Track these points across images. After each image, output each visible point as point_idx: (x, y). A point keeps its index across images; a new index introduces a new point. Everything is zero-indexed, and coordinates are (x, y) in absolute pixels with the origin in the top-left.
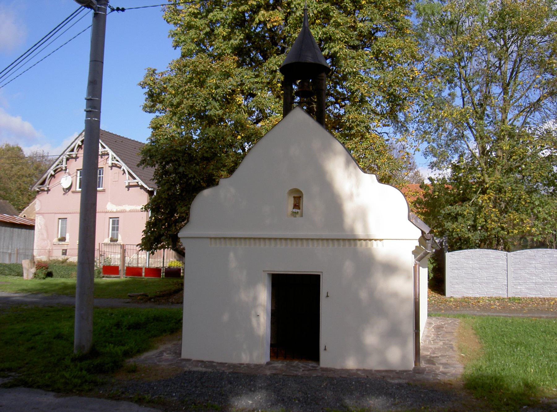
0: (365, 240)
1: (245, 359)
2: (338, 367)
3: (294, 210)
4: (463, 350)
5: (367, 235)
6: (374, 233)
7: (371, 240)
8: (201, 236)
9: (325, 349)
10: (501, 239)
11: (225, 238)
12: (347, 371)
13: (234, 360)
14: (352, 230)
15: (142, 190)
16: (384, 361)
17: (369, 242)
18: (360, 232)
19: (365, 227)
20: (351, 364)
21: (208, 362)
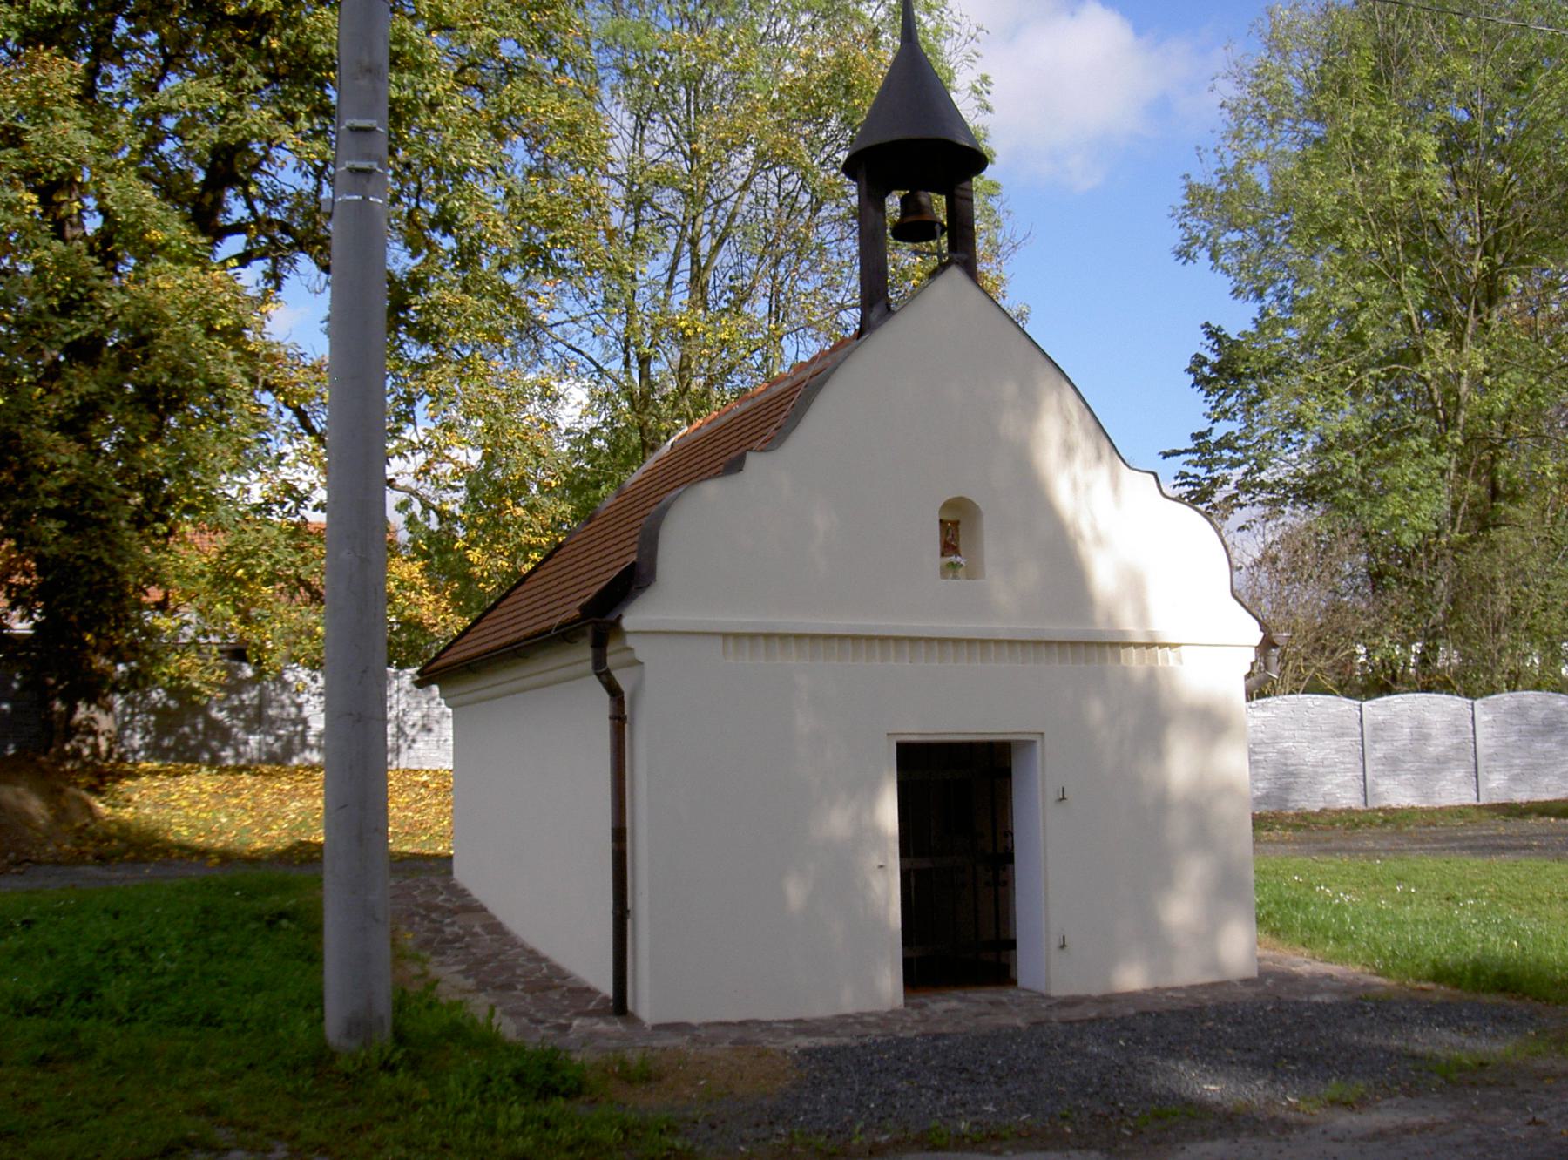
0: (1149, 645)
1: (848, 1002)
2: (1096, 990)
3: (947, 560)
4: (1539, 894)
5: (1151, 634)
6: (1164, 625)
7: (1149, 645)
8: (656, 629)
9: (1063, 946)
10: (258, 687)
11: (768, 636)
12: (1131, 997)
13: (818, 1008)
14: (1110, 618)
15: (753, 461)
16: (1215, 964)
17: (1160, 652)
18: (1129, 624)
19: (1142, 616)
20: (1132, 978)
21: (707, 1025)
